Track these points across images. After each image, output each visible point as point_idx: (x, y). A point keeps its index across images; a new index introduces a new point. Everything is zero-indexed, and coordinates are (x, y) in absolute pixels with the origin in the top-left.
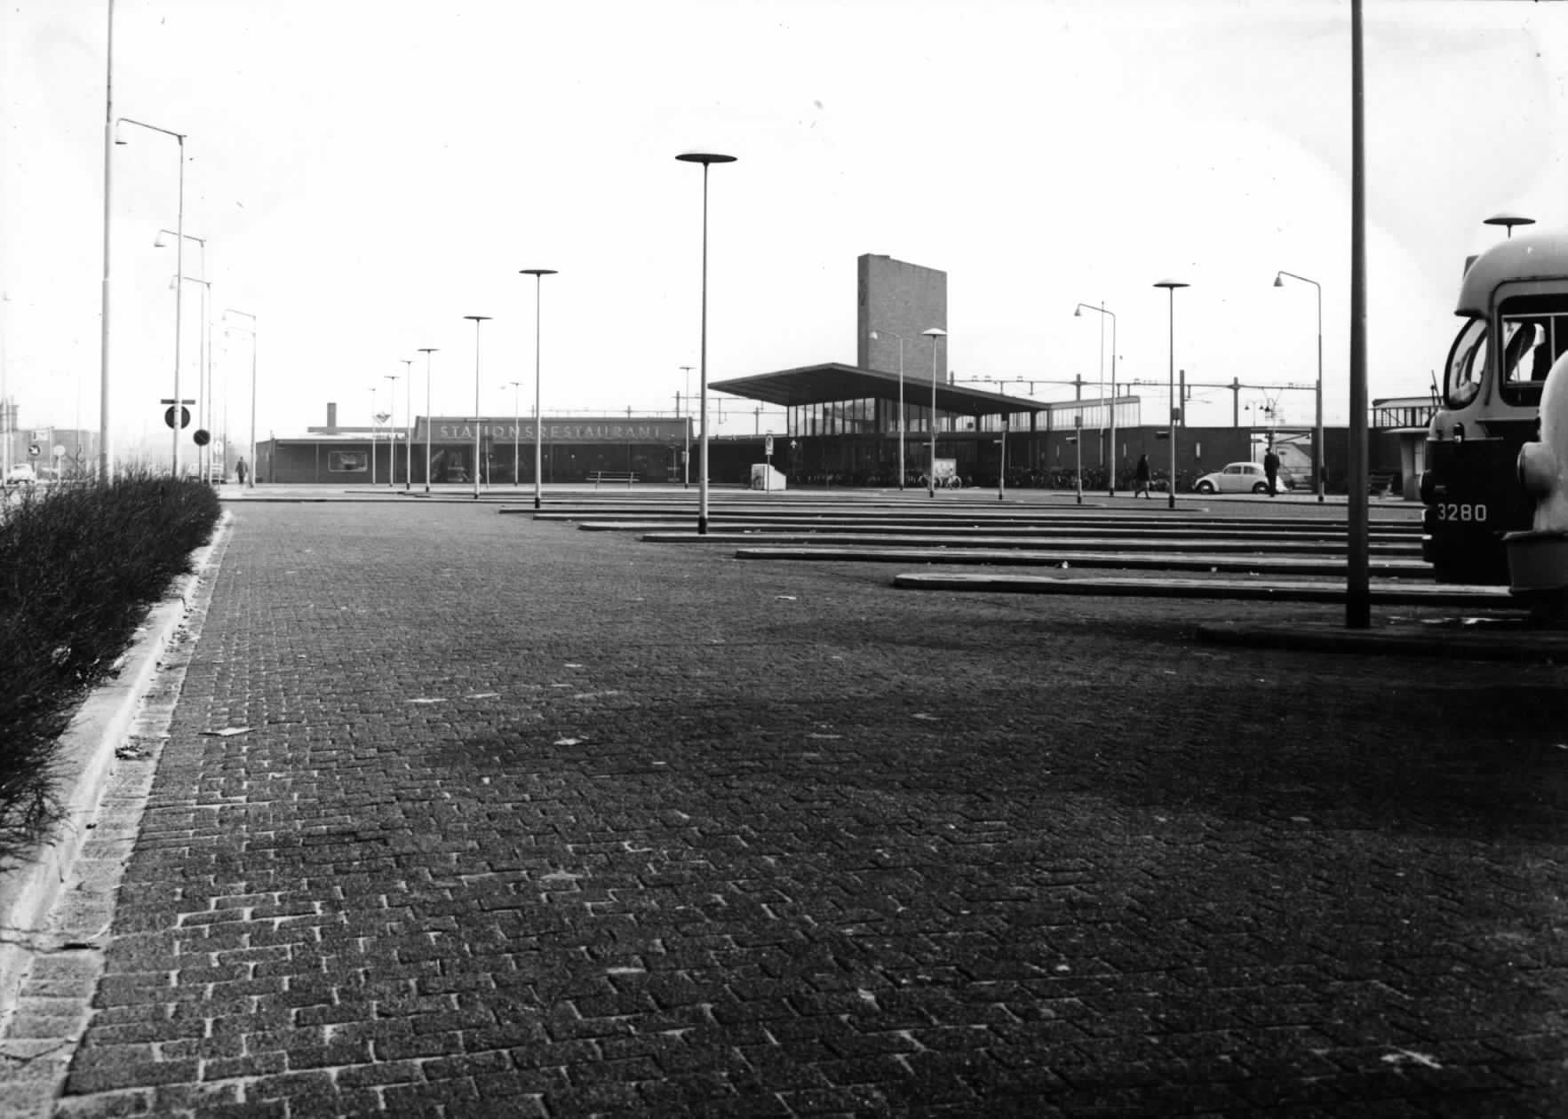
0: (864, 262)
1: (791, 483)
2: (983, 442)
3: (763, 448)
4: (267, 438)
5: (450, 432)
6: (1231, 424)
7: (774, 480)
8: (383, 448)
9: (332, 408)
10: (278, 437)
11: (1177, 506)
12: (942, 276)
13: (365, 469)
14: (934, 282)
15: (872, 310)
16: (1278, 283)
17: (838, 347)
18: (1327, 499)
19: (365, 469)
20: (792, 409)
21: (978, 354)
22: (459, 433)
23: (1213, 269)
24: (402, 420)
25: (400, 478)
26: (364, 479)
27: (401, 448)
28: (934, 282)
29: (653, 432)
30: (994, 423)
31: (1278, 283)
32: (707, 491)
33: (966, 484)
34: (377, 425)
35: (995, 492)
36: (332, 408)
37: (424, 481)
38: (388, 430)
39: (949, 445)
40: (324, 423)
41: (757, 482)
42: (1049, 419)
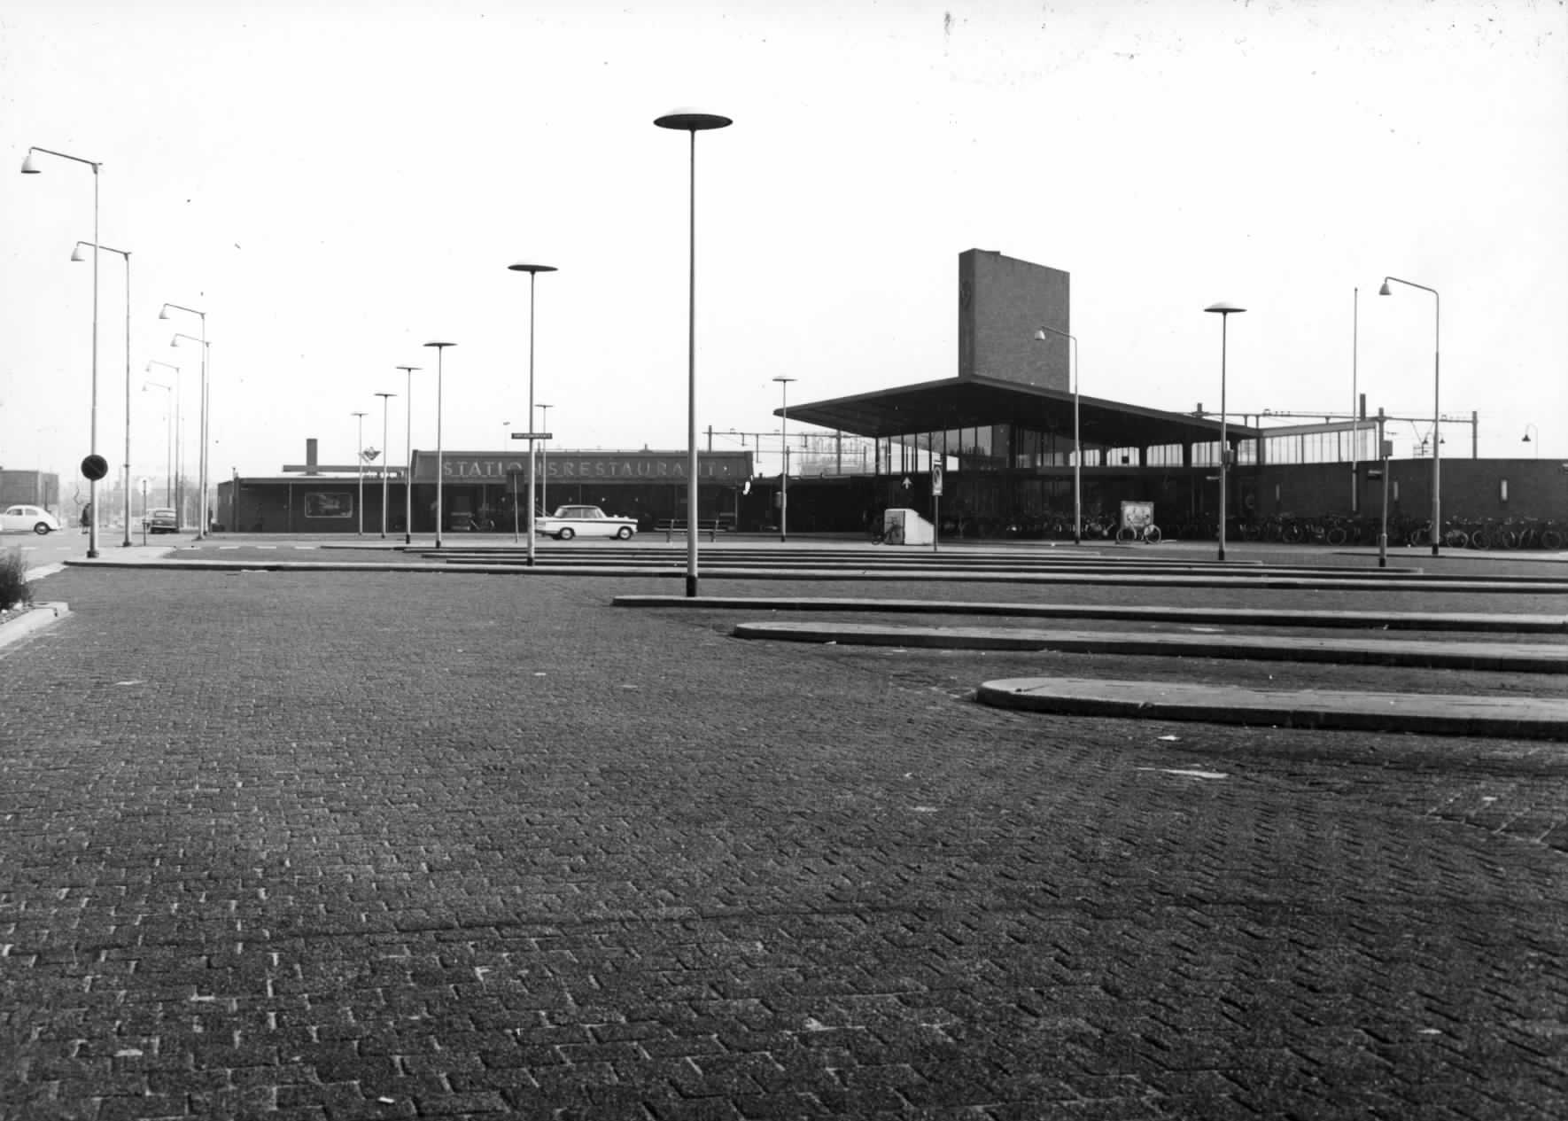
0: (968, 260)
1: (943, 535)
2: (1187, 475)
3: (930, 488)
4: (231, 478)
5: (608, 469)
6: (1470, 456)
7: (917, 530)
8: (373, 488)
9: (312, 445)
10: (244, 474)
11: (1376, 560)
12: (1063, 278)
13: (350, 515)
14: (1053, 285)
15: (978, 318)
16: (1384, 291)
17: (935, 360)
18: (451, 542)
19: (350, 515)
20: (883, 442)
21: (1101, 369)
22: (466, 470)
23: (1313, 280)
24: (396, 457)
25: (397, 525)
26: (349, 527)
27: (397, 489)
28: (1053, 285)
29: (576, 470)
30: (1206, 454)
31: (1384, 291)
32: (697, 545)
33: (1167, 535)
34: (364, 464)
35: (1212, 548)
36: (312, 445)
37: (433, 529)
38: (379, 469)
39: (1142, 483)
40: (303, 461)
41: (896, 534)
42: (1260, 451)
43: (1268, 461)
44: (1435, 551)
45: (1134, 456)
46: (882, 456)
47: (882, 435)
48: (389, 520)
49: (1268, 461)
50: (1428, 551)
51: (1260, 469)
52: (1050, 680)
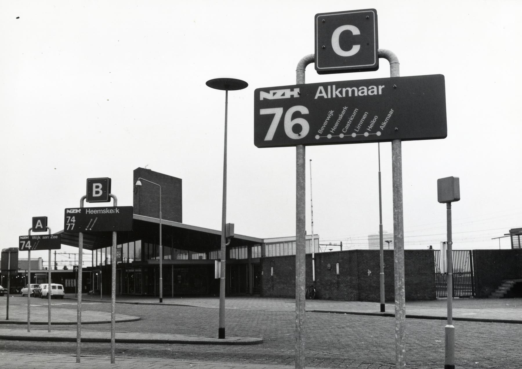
20: (95, 252)
21: (198, 213)
43: (267, 255)
44: (161, 301)
45: (204, 256)
46: (190, 257)
47: (94, 249)
48: (292, 274)
49: (267, 255)
50: (158, 301)
51: (263, 259)
52: (158, 359)
